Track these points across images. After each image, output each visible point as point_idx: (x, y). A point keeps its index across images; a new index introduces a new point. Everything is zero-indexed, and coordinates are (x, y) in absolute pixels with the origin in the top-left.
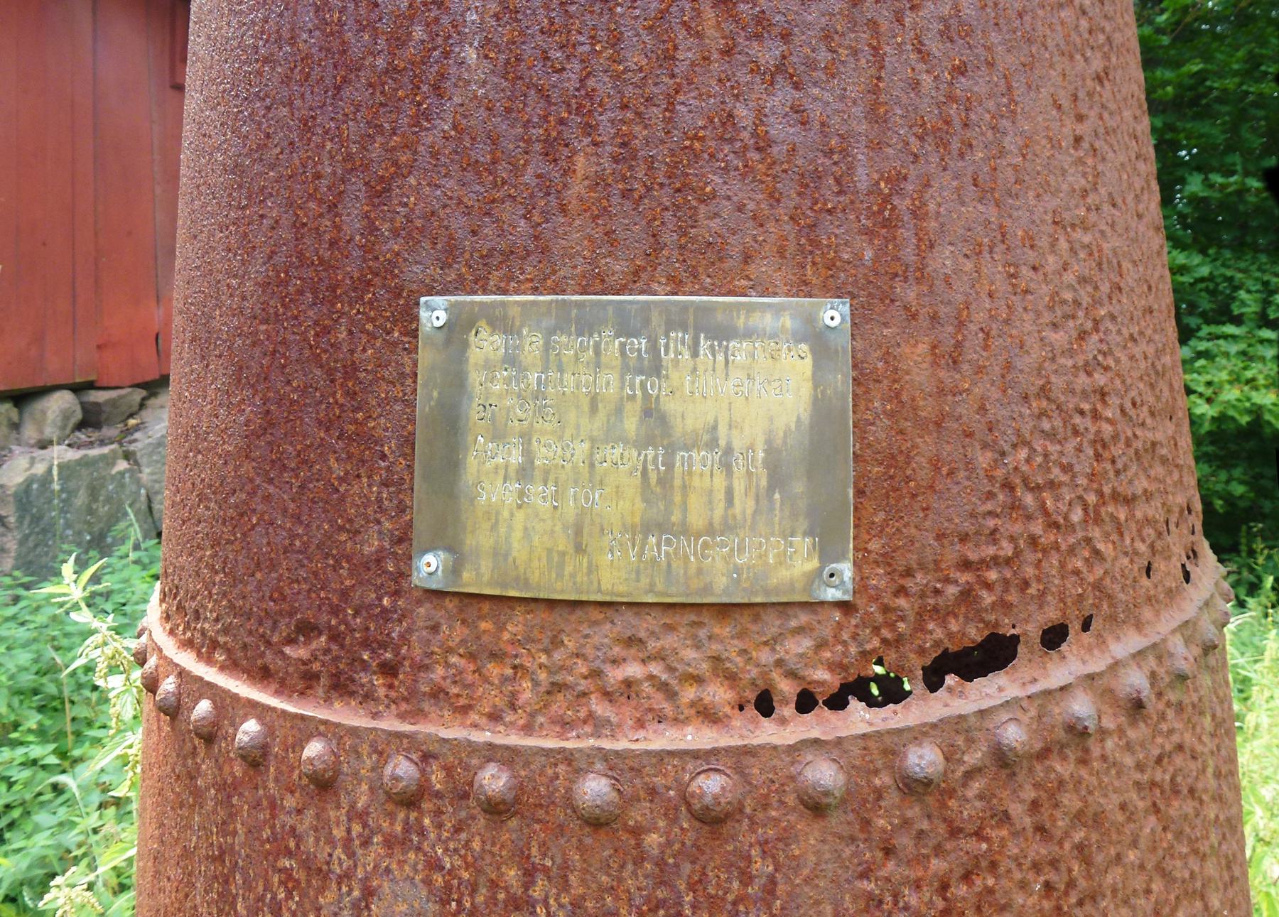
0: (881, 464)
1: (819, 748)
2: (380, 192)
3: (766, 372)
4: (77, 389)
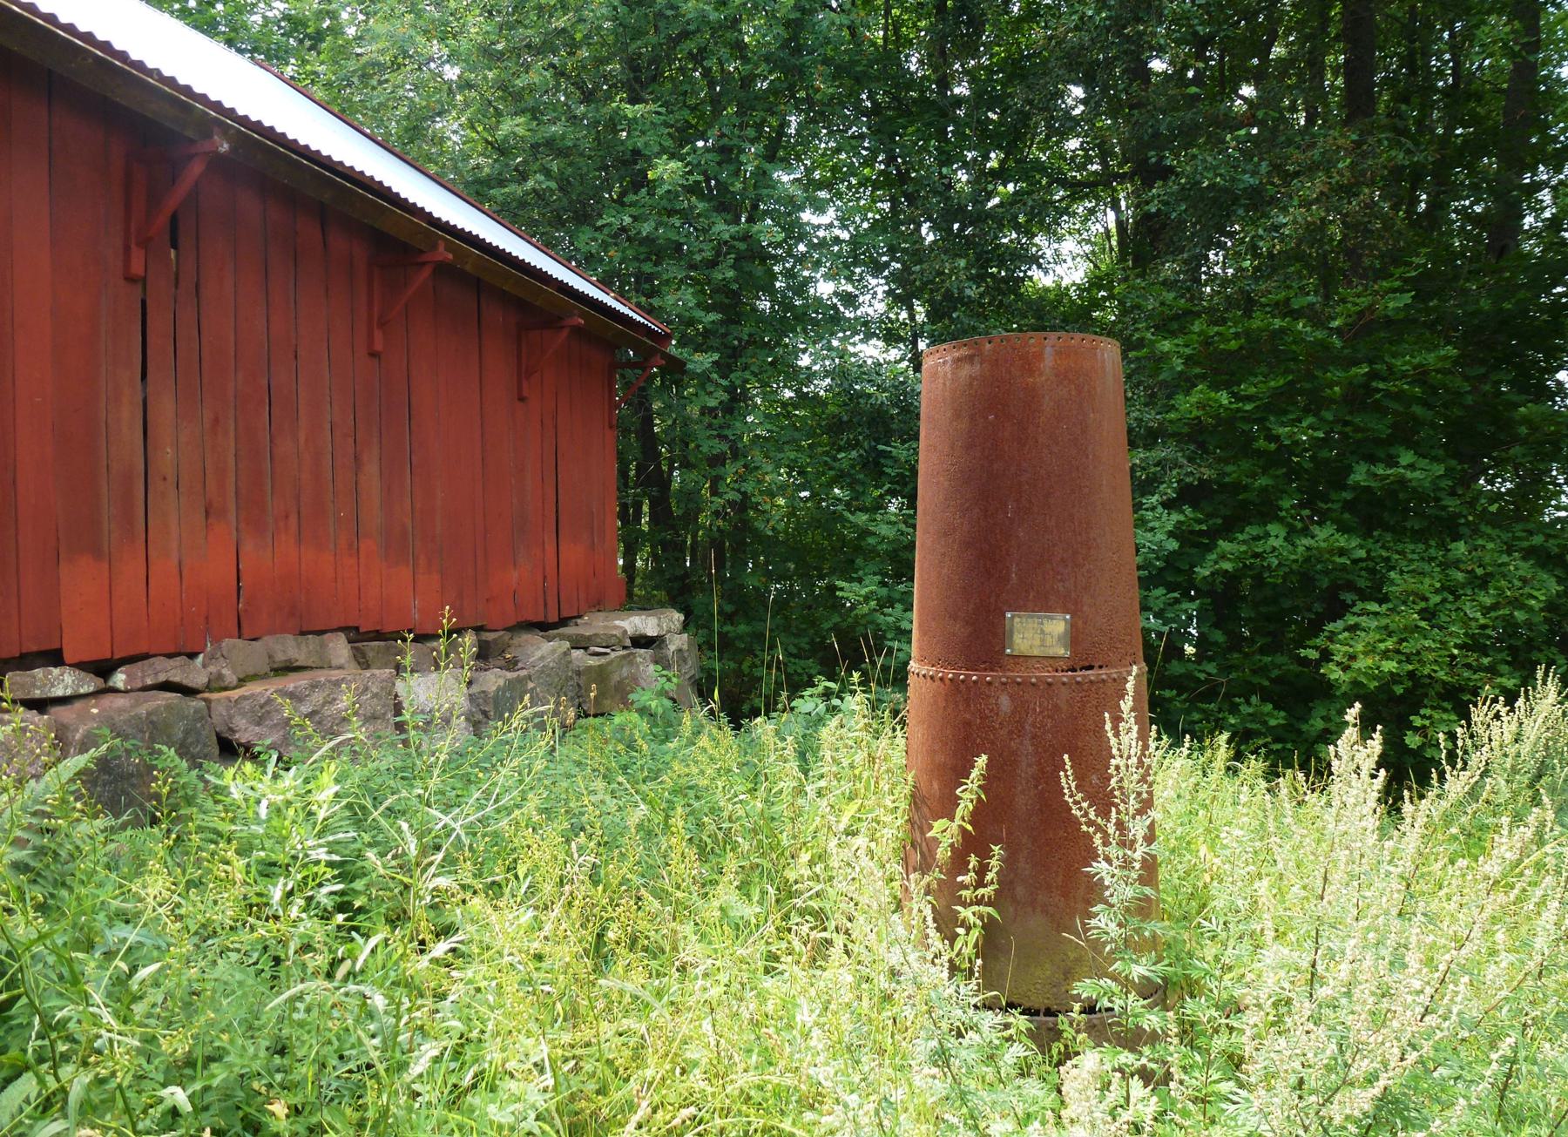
0: (1074, 638)
1: (1065, 677)
2: (998, 596)
3: (1057, 626)
4: (478, 629)
